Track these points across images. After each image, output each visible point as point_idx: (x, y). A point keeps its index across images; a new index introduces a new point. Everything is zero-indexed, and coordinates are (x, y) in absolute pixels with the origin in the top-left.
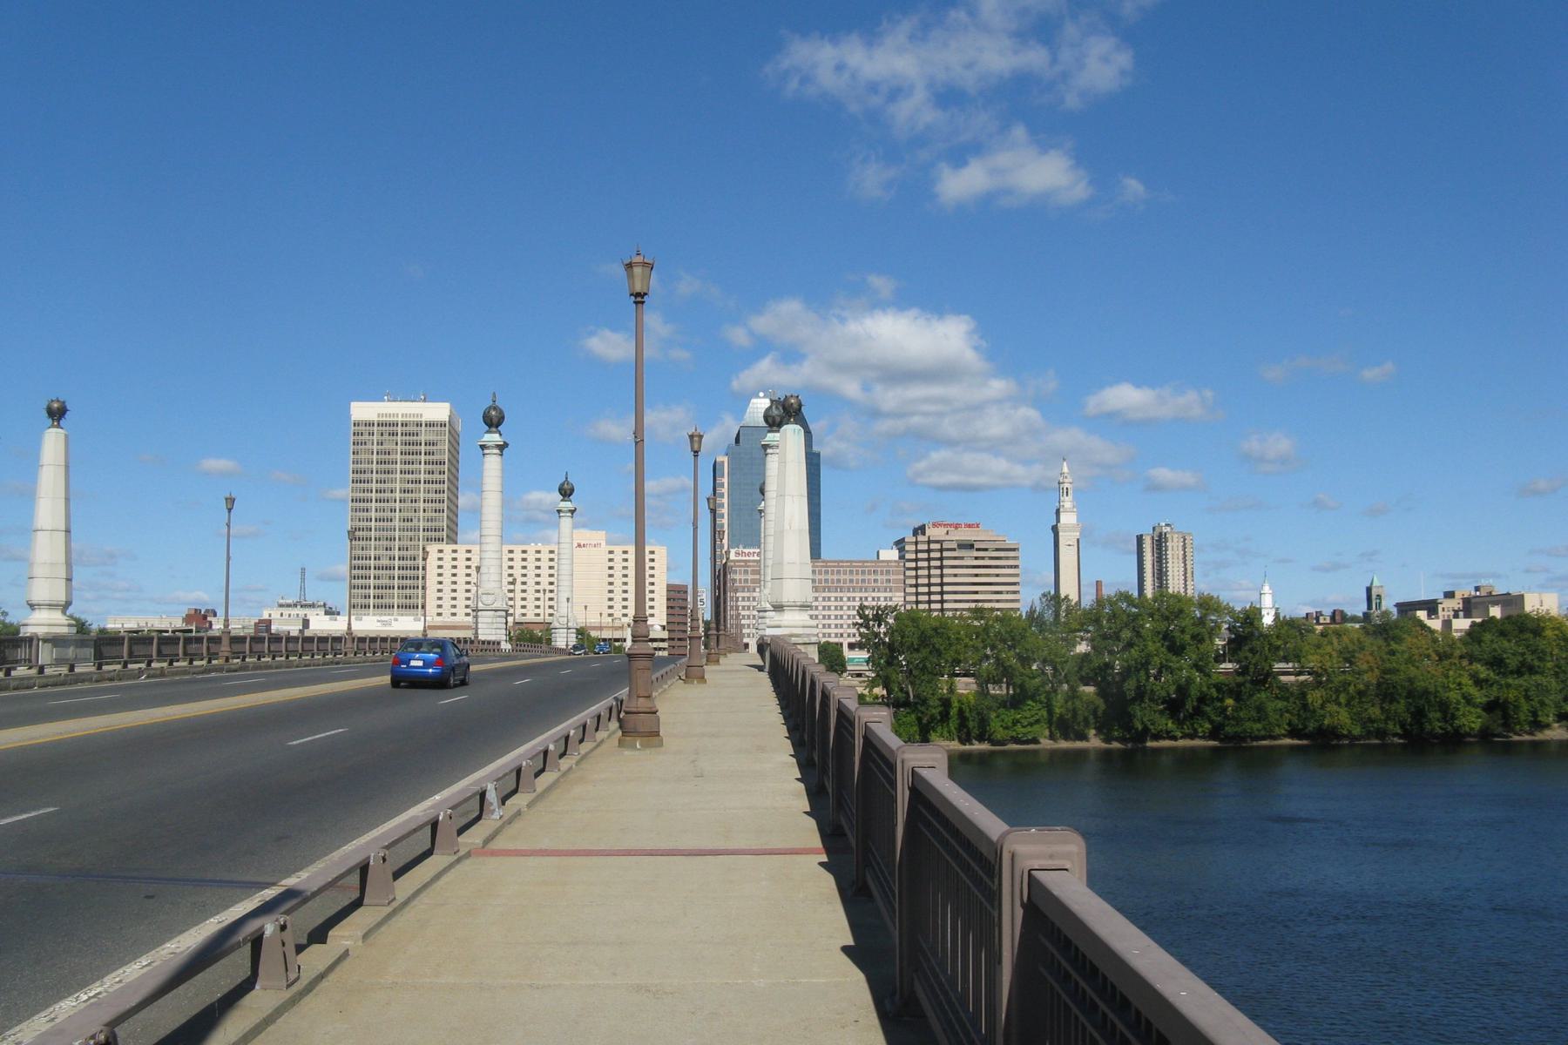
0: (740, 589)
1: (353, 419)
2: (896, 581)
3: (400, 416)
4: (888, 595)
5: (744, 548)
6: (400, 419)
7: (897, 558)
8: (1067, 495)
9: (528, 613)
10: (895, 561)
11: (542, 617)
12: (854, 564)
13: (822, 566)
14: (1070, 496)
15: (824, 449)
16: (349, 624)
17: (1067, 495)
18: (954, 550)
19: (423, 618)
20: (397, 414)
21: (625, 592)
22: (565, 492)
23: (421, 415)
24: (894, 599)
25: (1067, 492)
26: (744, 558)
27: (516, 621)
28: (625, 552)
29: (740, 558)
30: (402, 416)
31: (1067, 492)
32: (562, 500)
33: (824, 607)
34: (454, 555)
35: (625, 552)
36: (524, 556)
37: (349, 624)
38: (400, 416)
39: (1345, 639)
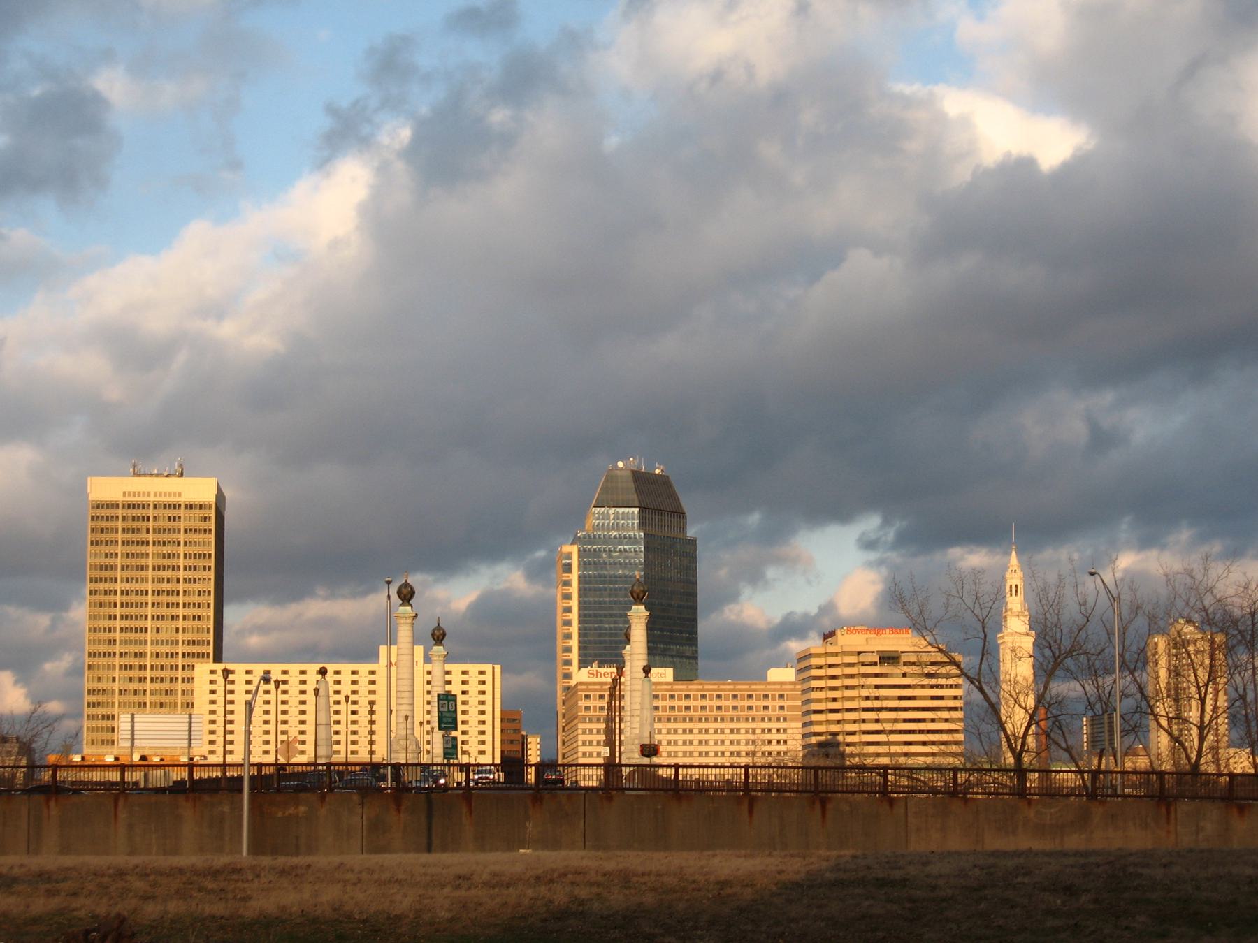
0: (594, 719)
1: (90, 499)
2: (791, 708)
3: (152, 495)
4: (782, 725)
5: (599, 667)
6: (152, 499)
7: (793, 679)
8: (1016, 594)
9: (360, 751)
10: (791, 683)
11: (343, 755)
12: (591, 687)
13: (698, 690)
14: (1021, 597)
15: (1093, 584)
16: (347, 758)
17: (1016, 594)
18: (875, 664)
19: (1191, 725)
20: (149, 493)
21: (303, 722)
22: (405, 596)
23: (180, 494)
24: (788, 731)
25: (1016, 591)
26: (599, 680)
27: (251, 763)
28: (482, 673)
29: (595, 680)
30: (155, 495)
31: (1016, 591)
32: (401, 605)
33: (700, 742)
34: (372, 677)
35: (482, 673)
36: (355, 677)
37: (347, 758)
38: (152, 495)
39: (649, 884)
